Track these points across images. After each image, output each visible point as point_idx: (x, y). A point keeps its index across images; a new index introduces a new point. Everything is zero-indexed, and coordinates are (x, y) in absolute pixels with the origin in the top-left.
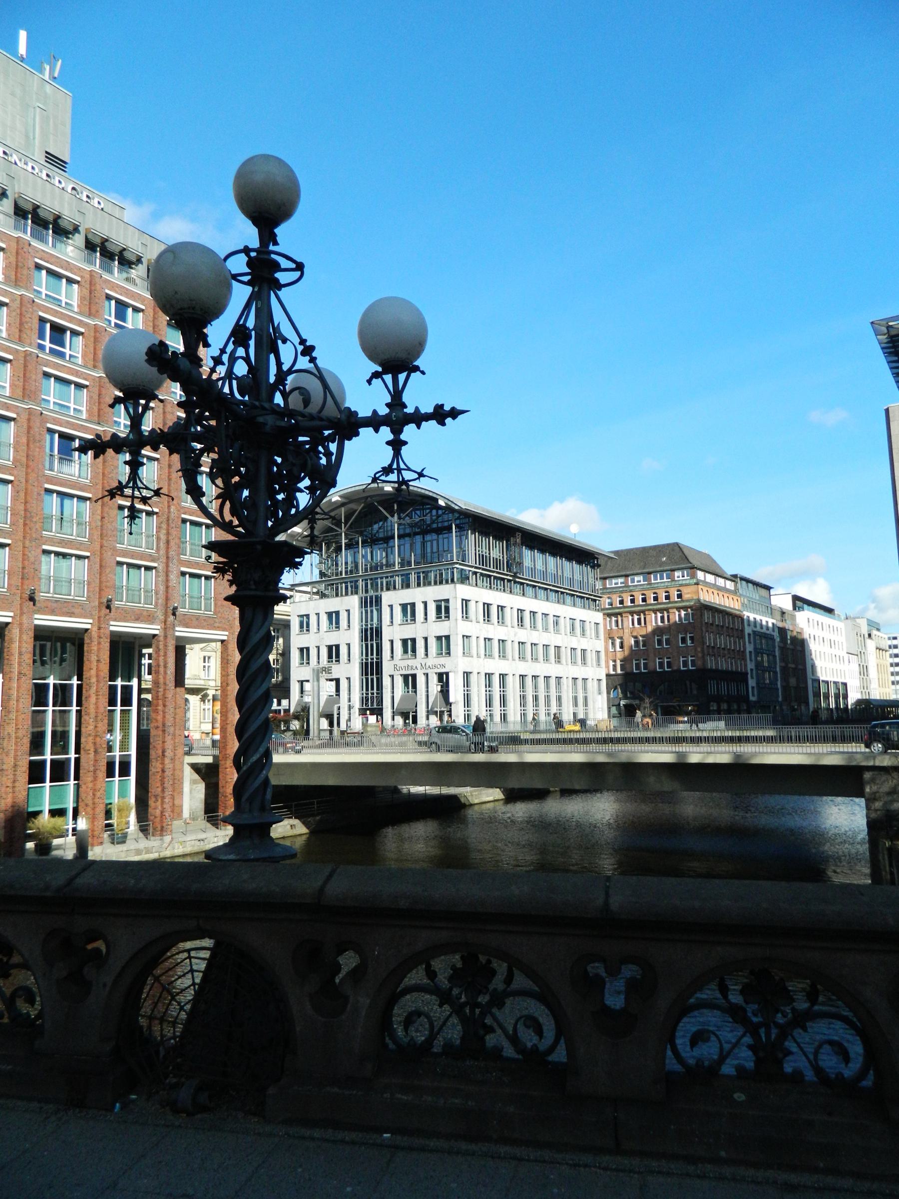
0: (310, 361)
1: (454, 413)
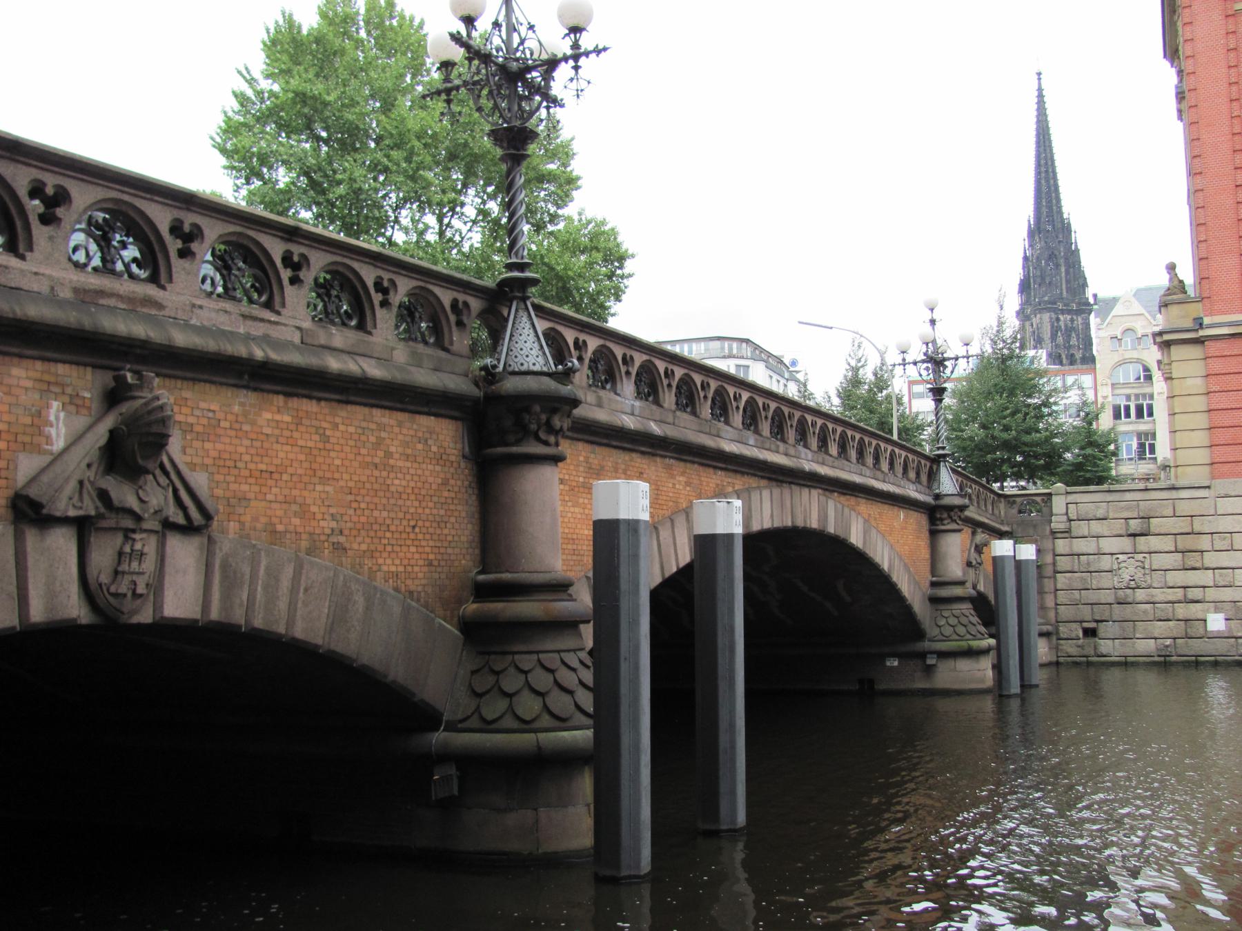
0: (566, 62)
1: (605, 49)
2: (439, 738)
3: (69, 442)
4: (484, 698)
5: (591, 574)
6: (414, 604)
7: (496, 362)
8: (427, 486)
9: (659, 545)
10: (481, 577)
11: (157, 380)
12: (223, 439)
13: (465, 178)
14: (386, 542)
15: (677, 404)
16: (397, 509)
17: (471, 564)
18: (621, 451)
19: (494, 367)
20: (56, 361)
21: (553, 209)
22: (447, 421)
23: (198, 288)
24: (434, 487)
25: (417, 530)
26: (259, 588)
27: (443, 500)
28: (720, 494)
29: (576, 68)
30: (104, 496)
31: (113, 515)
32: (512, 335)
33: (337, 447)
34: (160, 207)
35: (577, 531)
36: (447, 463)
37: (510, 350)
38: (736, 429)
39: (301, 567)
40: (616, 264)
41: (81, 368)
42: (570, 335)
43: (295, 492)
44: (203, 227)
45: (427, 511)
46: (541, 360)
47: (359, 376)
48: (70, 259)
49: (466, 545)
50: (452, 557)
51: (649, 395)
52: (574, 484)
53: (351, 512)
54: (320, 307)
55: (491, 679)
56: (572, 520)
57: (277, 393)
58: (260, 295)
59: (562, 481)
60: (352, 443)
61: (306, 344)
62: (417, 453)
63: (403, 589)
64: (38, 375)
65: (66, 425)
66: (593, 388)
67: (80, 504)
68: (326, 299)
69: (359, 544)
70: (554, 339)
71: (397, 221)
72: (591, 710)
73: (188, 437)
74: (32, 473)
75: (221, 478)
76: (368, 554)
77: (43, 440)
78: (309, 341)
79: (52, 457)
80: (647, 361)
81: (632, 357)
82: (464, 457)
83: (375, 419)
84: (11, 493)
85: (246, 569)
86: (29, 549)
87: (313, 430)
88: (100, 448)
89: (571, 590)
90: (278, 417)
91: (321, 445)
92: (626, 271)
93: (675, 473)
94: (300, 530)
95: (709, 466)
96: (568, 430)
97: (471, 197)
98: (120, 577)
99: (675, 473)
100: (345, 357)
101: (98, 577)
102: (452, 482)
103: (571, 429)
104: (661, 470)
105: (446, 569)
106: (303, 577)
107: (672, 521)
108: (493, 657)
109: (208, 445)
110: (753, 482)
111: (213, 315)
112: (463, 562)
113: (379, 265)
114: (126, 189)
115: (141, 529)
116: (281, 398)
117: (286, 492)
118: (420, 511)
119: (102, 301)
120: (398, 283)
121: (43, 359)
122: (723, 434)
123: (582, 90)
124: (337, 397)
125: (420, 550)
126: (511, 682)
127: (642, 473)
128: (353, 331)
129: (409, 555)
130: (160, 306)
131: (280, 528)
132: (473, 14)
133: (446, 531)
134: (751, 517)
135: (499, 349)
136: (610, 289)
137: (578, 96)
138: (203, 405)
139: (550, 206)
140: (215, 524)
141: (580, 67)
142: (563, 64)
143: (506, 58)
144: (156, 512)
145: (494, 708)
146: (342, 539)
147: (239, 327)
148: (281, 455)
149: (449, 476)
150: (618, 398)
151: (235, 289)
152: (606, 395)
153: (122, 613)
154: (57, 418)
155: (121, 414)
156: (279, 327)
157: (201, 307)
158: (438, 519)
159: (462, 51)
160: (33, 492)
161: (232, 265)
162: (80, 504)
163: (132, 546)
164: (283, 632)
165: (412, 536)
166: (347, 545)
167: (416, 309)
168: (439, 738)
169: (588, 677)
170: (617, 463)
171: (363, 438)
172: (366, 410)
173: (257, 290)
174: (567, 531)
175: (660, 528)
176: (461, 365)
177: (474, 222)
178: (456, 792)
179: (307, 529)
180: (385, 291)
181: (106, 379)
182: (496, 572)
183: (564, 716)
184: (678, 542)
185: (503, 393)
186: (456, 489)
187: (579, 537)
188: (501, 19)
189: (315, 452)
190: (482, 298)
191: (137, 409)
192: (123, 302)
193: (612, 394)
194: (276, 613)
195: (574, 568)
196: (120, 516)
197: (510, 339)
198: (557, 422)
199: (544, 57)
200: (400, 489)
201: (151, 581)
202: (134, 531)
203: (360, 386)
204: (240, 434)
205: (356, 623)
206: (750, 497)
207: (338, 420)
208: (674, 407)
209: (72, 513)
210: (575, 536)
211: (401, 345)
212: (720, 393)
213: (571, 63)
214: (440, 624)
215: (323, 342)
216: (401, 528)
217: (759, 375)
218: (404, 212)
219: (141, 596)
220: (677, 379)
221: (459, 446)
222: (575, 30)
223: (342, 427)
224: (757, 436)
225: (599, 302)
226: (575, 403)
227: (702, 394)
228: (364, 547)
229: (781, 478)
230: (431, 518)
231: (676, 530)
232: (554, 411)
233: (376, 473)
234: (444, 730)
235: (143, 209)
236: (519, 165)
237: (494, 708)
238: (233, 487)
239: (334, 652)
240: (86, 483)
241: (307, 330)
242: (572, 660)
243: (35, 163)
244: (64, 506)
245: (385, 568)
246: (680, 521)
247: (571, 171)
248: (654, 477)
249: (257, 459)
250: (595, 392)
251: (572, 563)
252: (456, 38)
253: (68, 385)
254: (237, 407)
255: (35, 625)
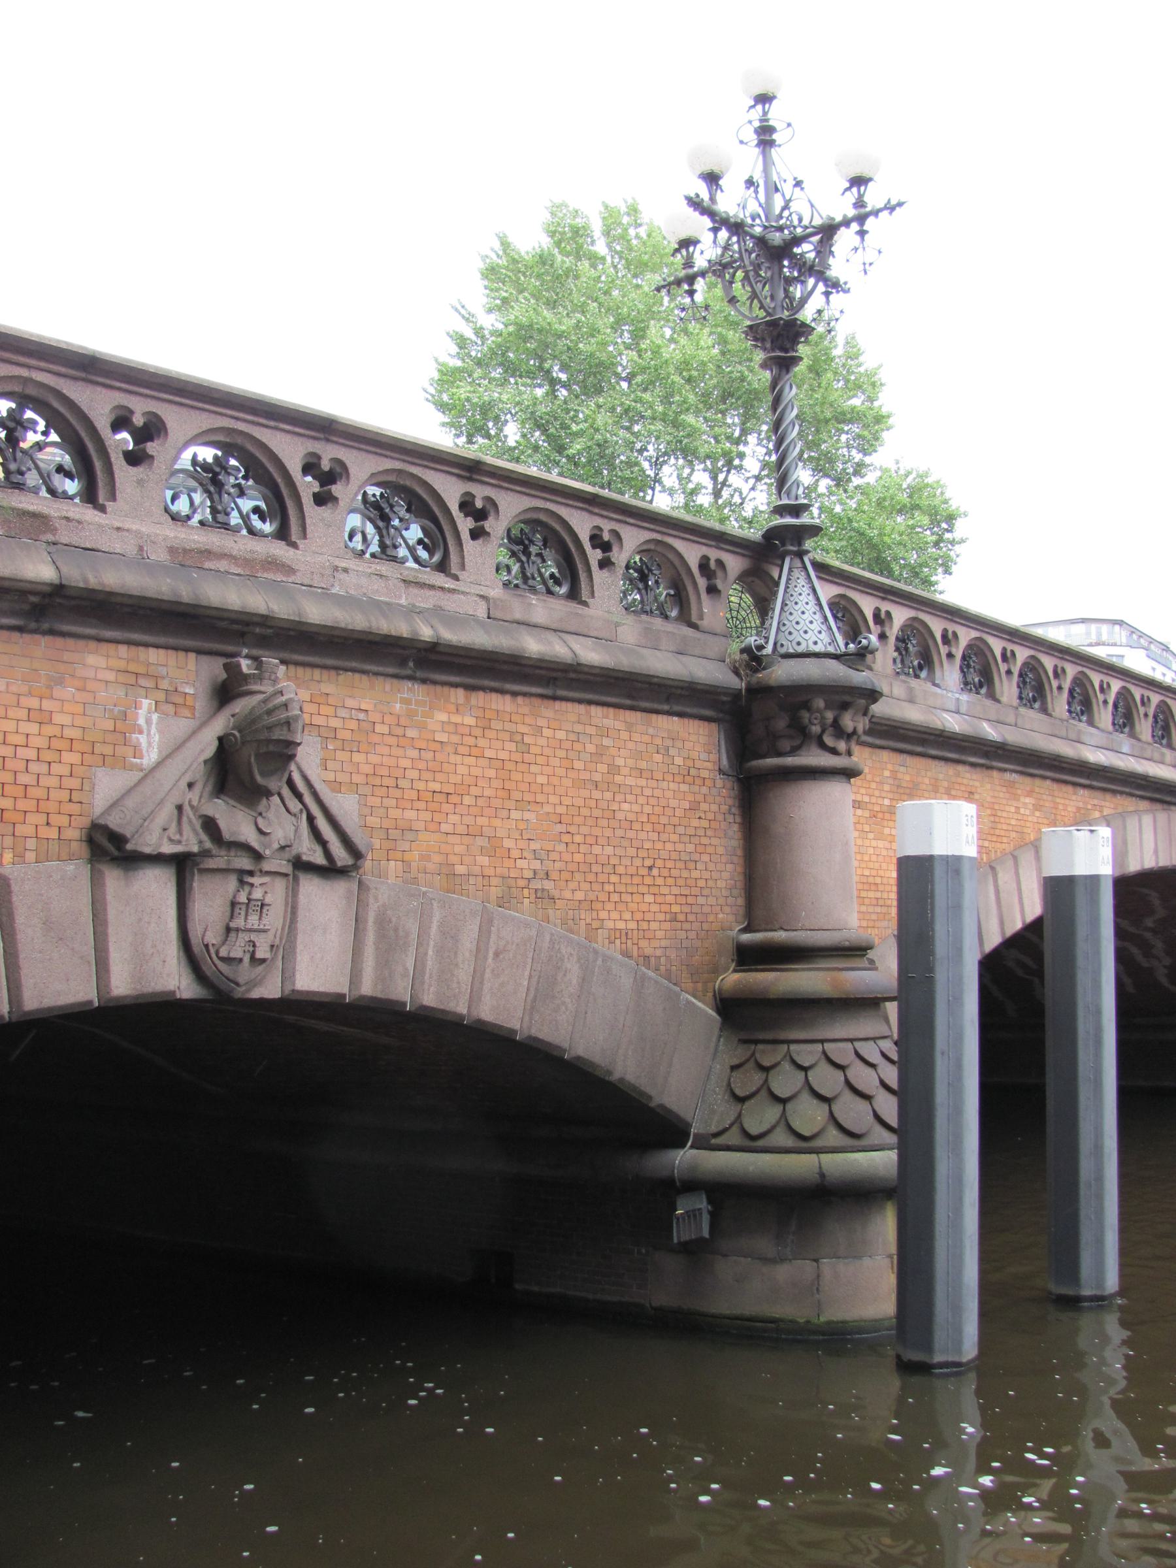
1: (900, 204)
2: (683, 1159)
3: (164, 754)
4: (747, 1104)
5: (896, 933)
6: (650, 973)
7: (762, 642)
8: (669, 812)
9: (997, 892)
10: (746, 937)
11: (283, 668)
12: (379, 749)
13: (744, 423)
14: (611, 888)
15: (1020, 698)
16: (626, 843)
17: (731, 918)
18: (942, 763)
19: (761, 648)
20: (146, 645)
21: (857, 456)
22: (697, 722)
23: (342, 545)
24: (679, 813)
25: (655, 872)
26: (430, 953)
27: (691, 831)
28: (1082, 820)
29: (862, 233)
30: (210, 826)
31: (223, 853)
32: (784, 604)
33: (540, 760)
34: (288, 437)
35: (881, 873)
36: (698, 781)
37: (781, 624)
38: (1103, 731)
39: (490, 922)
40: (944, 525)
41: (181, 654)
42: (867, 605)
43: (481, 821)
44: (349, 464)
45: (669, 846)
46: (825, 637)
47: (569, 661)
48: (167, 510)
49: (725, 893)
50: (706, 909)
51: (981, 685)
52: (877, 808)
53: (562, 848)
54: (516, 568)
55: (758, 1078)
56: (874, 858)
57: (456, 686)
58: (431, 554)
59: (857, 805)
60: (562, 754)
61: (495, 619)
62: (655, 768)
63: (635, 954)
64: (122, 664)
65: (160, 731)
66: (903, 677)
67: (177, 837)
68: (524, 559)
69: (573, 891)
70: (845, 609)
71: (657, 480)
72: (894, 1122)
73: (330, 747)
74: (115, 796)
75: (376, 801)
76: (586, 905)
77: (129, 751)
78: (495, 613)
79: (142, 774)
80: (976, 639)
81: (955, 634)
82: (720, 771)
83: (594, 721)
84: (85, 822)
85: (413, 927)
86: (109, 898)
87: (506, 736)
88: (205, 762)
89: (871, 954)
90: (456, 719)
91: (517, 757)
92: (957, 534)
93: (1019, 792)
94: (491, 872)
95: (1065, 782)
96: (865, 733)
97: (751, 446)
98: (233, 935)
99: (1019, 792)
100: (550, 636)
101: (203, 936)
102: (704, 806)
103: (870, 732)
104: (998, 788)
105: (696, 926)
106: (493, 937)
107: (1015, 858)
108: (760, 1047)
109: (357, 758)
110: (1129, 804)
111: (364, 581)
112: (721, 916)
113: (596, 510)
114: (241, 415)
115: (261, 871)
116: (460, 692)
117: (468, 820)
118: (659, 846)
119: (207, 565)
120: (623, 536)
121: (129, 643)
122: (1085, 738)
123: (871, 264)
124: (539, 690)
125: (660, 899)
126: (785, 1082)
127: (971, 793)
128: (563, 602)
129: (644, 907)
130: (289, 570)
131: (460, 869)
132: (716, 169)
133: (695, 874)
134: (1127, 852)
135: (767, 625)
136: (937, 559)
137: (866, 273)
138: (350, 703)
139: (854, 452)
140: (367, 864)
141: (866, 232)
142: (843, 229)
143: (765, 228)
144: (282, 848)
145: (761, 1117)
146: (548, 885)
147: (400, 597)
148: (462, 770)
149: (700, 798)
150: (938, 690)
151: (395, 547)
152: (920, 686)
153: (237, 984)
154: (148, 721)
155: (233, 716)
156: (456, 597)
157: (346, 570)
158: (684, 857)
159: (707, 222)
160: (114, 822)
161: (391, 515)
162: (177, 837)
163: (250, 894)
164: (465, 1012)
165: (648, 880)
166: (556, 894)
167: (650, 570)
168: (683, 1159)
169: (891, 1075)
170: (937, 780)
171: (577, 746)
172: (582, 708)
173: (426, 548)
174: (867, 873)
175: (998, 868)
176: (714, 646)
177: (758, 478)
178: (706, 1233)
179: (499, 870)
180: (606, 547)
181: (214, 669)
182: (766, 930)
183: (856, 1130)
184: (1023, 887)
185: (772, 683)
186: (710, 816)
187: (885, 881)
188: (758, 177)
189: (509, 766)
190: (743, 555)
191: (253, 708)
192: (237, 565)
193: (929, 684)
194: (455, 985)
195: (878, 924)
196: (232, 854)
197: (782, 609)
198: (848, 722)
199: (817, 222)
200: (631, 817)
201: (277, 942)
202: (251, 873)
203: (572, 675)
204: (402, 741)
205: (568, 1000)
206: (1125, 828)
207: (541, 722)
208: (1016, 702)
209: (168, 849)
210: (878, 880)
211: (630, 620)
212: (1080, 682)
213: (855, 227)
214: (689, 1002)
215: (518, 616)
216: (632, 870)
217: (1137, 662)
218: (666, 470)
219: (263, 961)
220: (1019, 662)
221: (714, 757)
222: (859, 181)
223: (547, 732)
224: (1134, 741)
225: (922, 575)
226: (873, 695)
227: (1055, 684)
228: (579, 895)
229: (1168, 799)
230: (674, 856)
231: (1021, 871)
232: (845, 706)
233: (597, 794)
234: (692, 1147)
235: (264, 440)
236: (788, 371)
237: (761, 1117)
238: (394, 813)
239: (536, 1039)
240: (187, 808)
241: (495, 600)
242: (870, 1051)
243: (118, 384)
244: (152, 841)
245: (609, 924)
246: (1027, 858)
247: (881, 407)
248: (989, 799)
249: (427, 775)
250: (904, 682)
251: (874, 917)
252: (695, 203)
253: (163, 678)
254: (398, 706)
255: (118, 998)
